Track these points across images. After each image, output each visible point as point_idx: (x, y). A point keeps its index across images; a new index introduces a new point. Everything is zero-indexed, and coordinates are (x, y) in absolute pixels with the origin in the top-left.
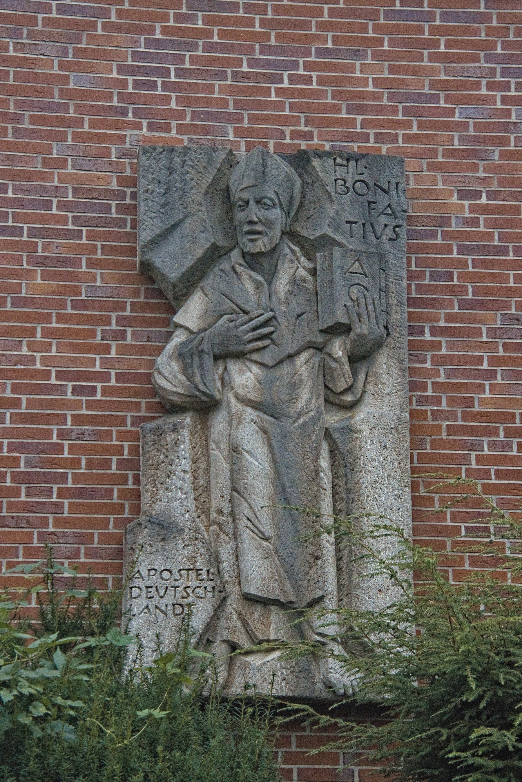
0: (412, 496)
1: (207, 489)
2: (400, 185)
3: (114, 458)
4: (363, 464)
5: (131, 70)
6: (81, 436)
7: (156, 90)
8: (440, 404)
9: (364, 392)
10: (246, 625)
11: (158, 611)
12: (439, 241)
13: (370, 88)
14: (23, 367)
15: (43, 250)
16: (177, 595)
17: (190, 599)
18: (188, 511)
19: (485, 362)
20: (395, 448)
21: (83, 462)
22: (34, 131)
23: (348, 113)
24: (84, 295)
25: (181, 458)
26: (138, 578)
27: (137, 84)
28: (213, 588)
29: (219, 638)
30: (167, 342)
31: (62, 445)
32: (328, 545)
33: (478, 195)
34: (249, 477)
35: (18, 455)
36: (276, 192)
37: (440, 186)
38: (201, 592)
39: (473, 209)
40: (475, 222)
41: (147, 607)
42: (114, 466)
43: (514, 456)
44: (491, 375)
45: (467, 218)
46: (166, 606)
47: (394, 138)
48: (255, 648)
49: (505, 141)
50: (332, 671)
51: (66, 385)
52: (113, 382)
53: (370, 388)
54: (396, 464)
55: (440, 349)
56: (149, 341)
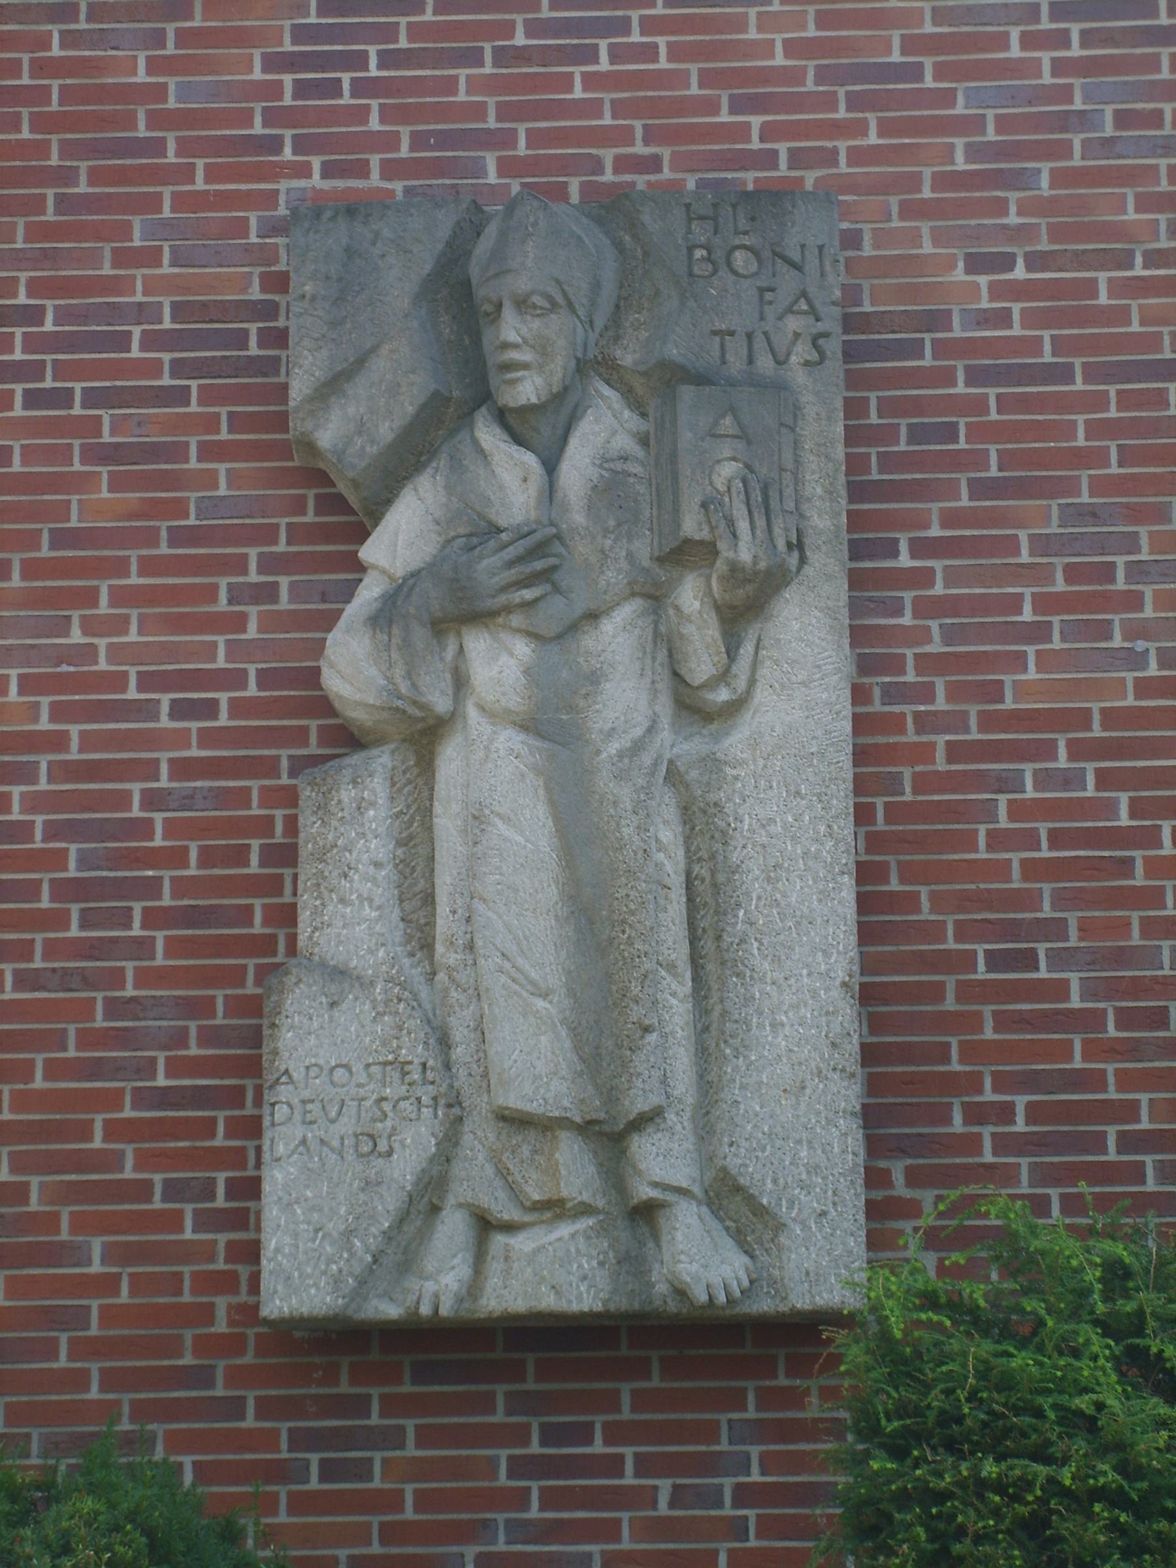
0: (858, 894)
1: (429, 899)
2: (826, 250)
3: (255, 844)
4: (748, 830)
5: (289, 62)
6: (188, 800)
7: (341, 96)
8: (930, 698)
9: (752, 682)
10: (505, 1172)
11: (325, 1149)
12: (928, 361)
13: (780, 60)
14: (72, 669)
15: (113, 432)
16: (363, 1114)
17: (389, 1123)
18: (383, 945)
19: (1027, 608)
20: (819, 795)
21: (193, 855)
22: (98, 197)
23: (733, 111)
24: (193, 515)
25: (370, 836)
26: (287, 1083)
27: (301, 89)
28: (435, 1099)
29: (451, 1200)
30: (348, 602)
31: (150, 821)
32: (674, 1002)
33: (1008, 263)
34: (505, 868)
35: (64, 845)
36: (558, 281)
37: (927, 248)
38: (410, 1108)
39: (997, 291)
40: (1003, 317)
41: (304, 1142)
42: (254, 859)
43: (1089, 798)
44: (1039, 632)
45: (985, 311)
46: (342, 1138)
47: (831, 158)
48: (527, 1218)
49: (1062, 150)
50: (683, 1257)
51: (158, 701)
52: (252, 690)
53: (766, 672)
54: (823, 829)
55: (932, 584)
56: (324, 601)
